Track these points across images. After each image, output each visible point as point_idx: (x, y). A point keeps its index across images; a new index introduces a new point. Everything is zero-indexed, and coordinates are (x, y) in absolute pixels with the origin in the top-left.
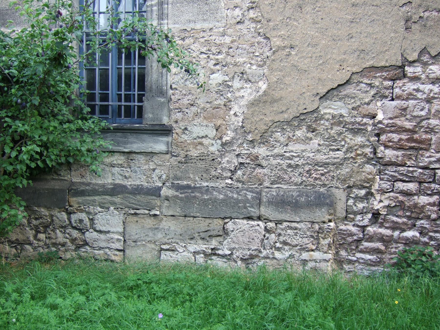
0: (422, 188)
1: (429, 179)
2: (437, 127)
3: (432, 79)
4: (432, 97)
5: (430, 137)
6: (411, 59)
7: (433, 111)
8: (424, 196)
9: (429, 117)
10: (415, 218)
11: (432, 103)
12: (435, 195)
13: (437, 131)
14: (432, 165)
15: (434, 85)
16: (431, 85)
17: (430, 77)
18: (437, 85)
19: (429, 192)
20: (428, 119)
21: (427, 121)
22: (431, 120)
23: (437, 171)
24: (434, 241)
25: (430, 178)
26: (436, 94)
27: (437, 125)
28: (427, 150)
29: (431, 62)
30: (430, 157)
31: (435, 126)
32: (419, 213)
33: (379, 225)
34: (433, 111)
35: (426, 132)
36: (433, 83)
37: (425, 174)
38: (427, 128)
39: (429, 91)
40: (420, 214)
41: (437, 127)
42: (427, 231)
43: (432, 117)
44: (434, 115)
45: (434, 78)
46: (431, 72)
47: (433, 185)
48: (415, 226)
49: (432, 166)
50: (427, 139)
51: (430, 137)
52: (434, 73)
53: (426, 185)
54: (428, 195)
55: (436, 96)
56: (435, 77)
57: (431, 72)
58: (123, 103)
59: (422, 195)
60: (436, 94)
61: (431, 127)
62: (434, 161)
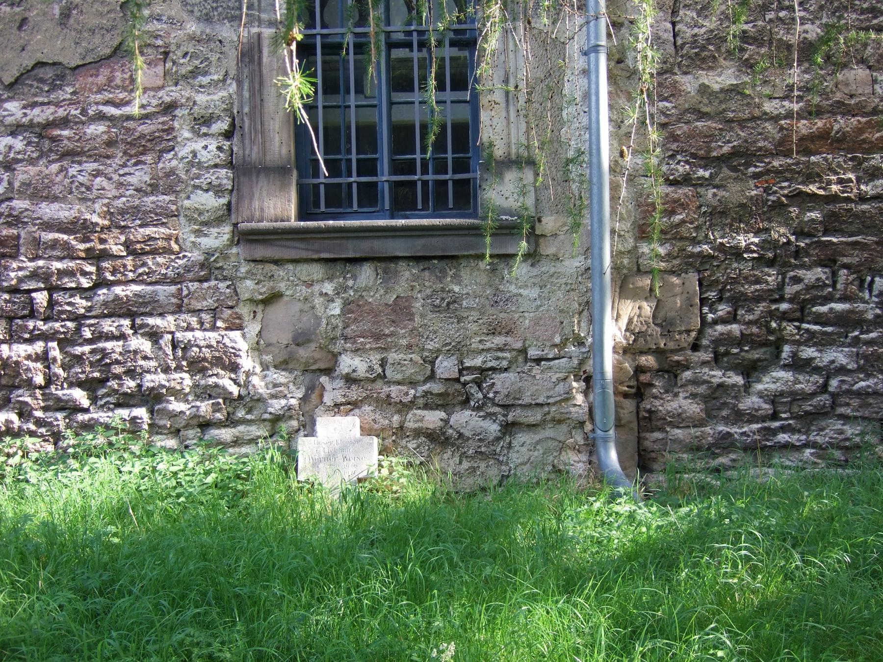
0: (14, 328)
1: (23, 310)
2: (25, 214)
3: (10, 125)
4: (13, 159)
5: (15, 232)
6: (73, 64)
7: (17, 184)
8: (19, 343)
9: (11, 195)
10: (8, 386)
11: (15, 169)
12: (38, 339)
13: (26, 220)
14: (23, 285)
15: (15, 138)
16: (10, 138)
17: (6, 123)
18: (21, 138)
19: (27, 336)
20: (10, 199)
21: (7, 203)
22: (15, 201)
23: (34, 295)
24: (44, 426)
25: (24, 308)
26: (19, 153)
27: (27, 210)
28: (14, 257)
29: (6, 96)
30: (20, 269)
31: (21, 213)
32: (14, 376)
33: (550, 426)
34: (17, 184)
35: (9, 225)
36: (13, 134)
37: (15, 302)
38: (10, 215)
39: (7, 148)
40: (16, 377)
41: (25, 214)
42: (29, 409)
43: (16, 196)
44: (19, 192)
45: (14, 125)
46: (6, 113)
47: (31, 324)
48: (9, 400)
49: (25, 287)
50: (11, 237)
51: (15, 232)
52: (11, 115)
53: (19, 322)
54: (26, 341)
55: (20, 157)
56: (15, 122)
57: (6, 113)
58: (318, 30)
59: (15, 342)
60: (19, 153)
61: (15, 213)
62: (26, 277)
